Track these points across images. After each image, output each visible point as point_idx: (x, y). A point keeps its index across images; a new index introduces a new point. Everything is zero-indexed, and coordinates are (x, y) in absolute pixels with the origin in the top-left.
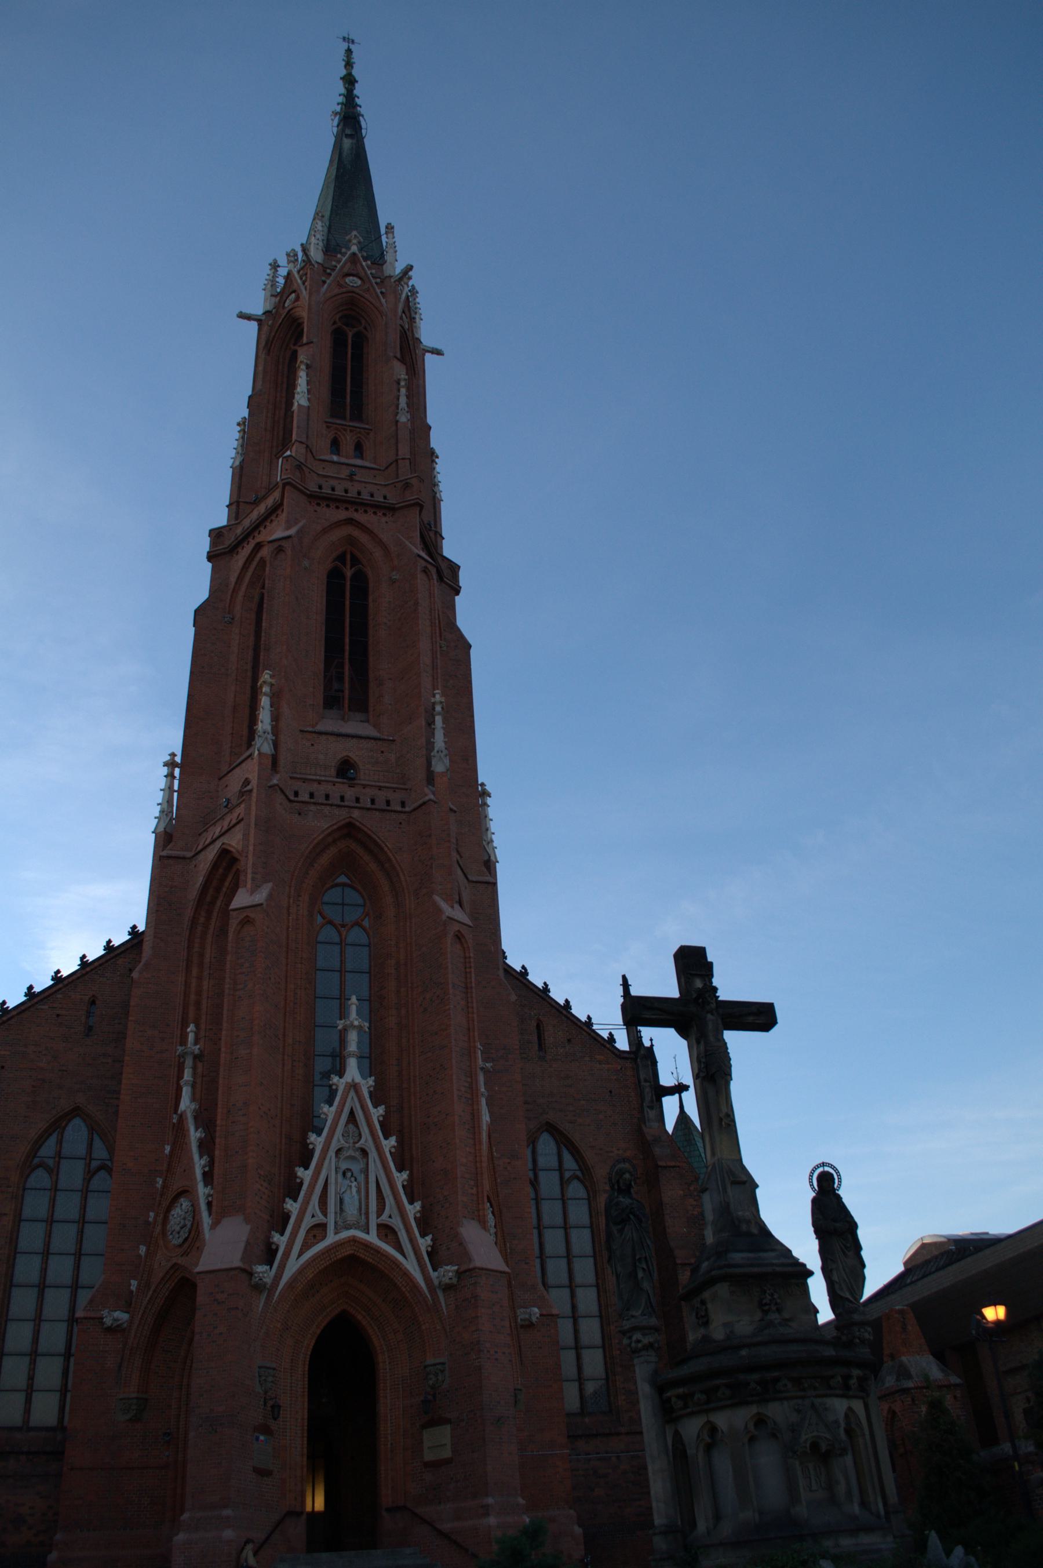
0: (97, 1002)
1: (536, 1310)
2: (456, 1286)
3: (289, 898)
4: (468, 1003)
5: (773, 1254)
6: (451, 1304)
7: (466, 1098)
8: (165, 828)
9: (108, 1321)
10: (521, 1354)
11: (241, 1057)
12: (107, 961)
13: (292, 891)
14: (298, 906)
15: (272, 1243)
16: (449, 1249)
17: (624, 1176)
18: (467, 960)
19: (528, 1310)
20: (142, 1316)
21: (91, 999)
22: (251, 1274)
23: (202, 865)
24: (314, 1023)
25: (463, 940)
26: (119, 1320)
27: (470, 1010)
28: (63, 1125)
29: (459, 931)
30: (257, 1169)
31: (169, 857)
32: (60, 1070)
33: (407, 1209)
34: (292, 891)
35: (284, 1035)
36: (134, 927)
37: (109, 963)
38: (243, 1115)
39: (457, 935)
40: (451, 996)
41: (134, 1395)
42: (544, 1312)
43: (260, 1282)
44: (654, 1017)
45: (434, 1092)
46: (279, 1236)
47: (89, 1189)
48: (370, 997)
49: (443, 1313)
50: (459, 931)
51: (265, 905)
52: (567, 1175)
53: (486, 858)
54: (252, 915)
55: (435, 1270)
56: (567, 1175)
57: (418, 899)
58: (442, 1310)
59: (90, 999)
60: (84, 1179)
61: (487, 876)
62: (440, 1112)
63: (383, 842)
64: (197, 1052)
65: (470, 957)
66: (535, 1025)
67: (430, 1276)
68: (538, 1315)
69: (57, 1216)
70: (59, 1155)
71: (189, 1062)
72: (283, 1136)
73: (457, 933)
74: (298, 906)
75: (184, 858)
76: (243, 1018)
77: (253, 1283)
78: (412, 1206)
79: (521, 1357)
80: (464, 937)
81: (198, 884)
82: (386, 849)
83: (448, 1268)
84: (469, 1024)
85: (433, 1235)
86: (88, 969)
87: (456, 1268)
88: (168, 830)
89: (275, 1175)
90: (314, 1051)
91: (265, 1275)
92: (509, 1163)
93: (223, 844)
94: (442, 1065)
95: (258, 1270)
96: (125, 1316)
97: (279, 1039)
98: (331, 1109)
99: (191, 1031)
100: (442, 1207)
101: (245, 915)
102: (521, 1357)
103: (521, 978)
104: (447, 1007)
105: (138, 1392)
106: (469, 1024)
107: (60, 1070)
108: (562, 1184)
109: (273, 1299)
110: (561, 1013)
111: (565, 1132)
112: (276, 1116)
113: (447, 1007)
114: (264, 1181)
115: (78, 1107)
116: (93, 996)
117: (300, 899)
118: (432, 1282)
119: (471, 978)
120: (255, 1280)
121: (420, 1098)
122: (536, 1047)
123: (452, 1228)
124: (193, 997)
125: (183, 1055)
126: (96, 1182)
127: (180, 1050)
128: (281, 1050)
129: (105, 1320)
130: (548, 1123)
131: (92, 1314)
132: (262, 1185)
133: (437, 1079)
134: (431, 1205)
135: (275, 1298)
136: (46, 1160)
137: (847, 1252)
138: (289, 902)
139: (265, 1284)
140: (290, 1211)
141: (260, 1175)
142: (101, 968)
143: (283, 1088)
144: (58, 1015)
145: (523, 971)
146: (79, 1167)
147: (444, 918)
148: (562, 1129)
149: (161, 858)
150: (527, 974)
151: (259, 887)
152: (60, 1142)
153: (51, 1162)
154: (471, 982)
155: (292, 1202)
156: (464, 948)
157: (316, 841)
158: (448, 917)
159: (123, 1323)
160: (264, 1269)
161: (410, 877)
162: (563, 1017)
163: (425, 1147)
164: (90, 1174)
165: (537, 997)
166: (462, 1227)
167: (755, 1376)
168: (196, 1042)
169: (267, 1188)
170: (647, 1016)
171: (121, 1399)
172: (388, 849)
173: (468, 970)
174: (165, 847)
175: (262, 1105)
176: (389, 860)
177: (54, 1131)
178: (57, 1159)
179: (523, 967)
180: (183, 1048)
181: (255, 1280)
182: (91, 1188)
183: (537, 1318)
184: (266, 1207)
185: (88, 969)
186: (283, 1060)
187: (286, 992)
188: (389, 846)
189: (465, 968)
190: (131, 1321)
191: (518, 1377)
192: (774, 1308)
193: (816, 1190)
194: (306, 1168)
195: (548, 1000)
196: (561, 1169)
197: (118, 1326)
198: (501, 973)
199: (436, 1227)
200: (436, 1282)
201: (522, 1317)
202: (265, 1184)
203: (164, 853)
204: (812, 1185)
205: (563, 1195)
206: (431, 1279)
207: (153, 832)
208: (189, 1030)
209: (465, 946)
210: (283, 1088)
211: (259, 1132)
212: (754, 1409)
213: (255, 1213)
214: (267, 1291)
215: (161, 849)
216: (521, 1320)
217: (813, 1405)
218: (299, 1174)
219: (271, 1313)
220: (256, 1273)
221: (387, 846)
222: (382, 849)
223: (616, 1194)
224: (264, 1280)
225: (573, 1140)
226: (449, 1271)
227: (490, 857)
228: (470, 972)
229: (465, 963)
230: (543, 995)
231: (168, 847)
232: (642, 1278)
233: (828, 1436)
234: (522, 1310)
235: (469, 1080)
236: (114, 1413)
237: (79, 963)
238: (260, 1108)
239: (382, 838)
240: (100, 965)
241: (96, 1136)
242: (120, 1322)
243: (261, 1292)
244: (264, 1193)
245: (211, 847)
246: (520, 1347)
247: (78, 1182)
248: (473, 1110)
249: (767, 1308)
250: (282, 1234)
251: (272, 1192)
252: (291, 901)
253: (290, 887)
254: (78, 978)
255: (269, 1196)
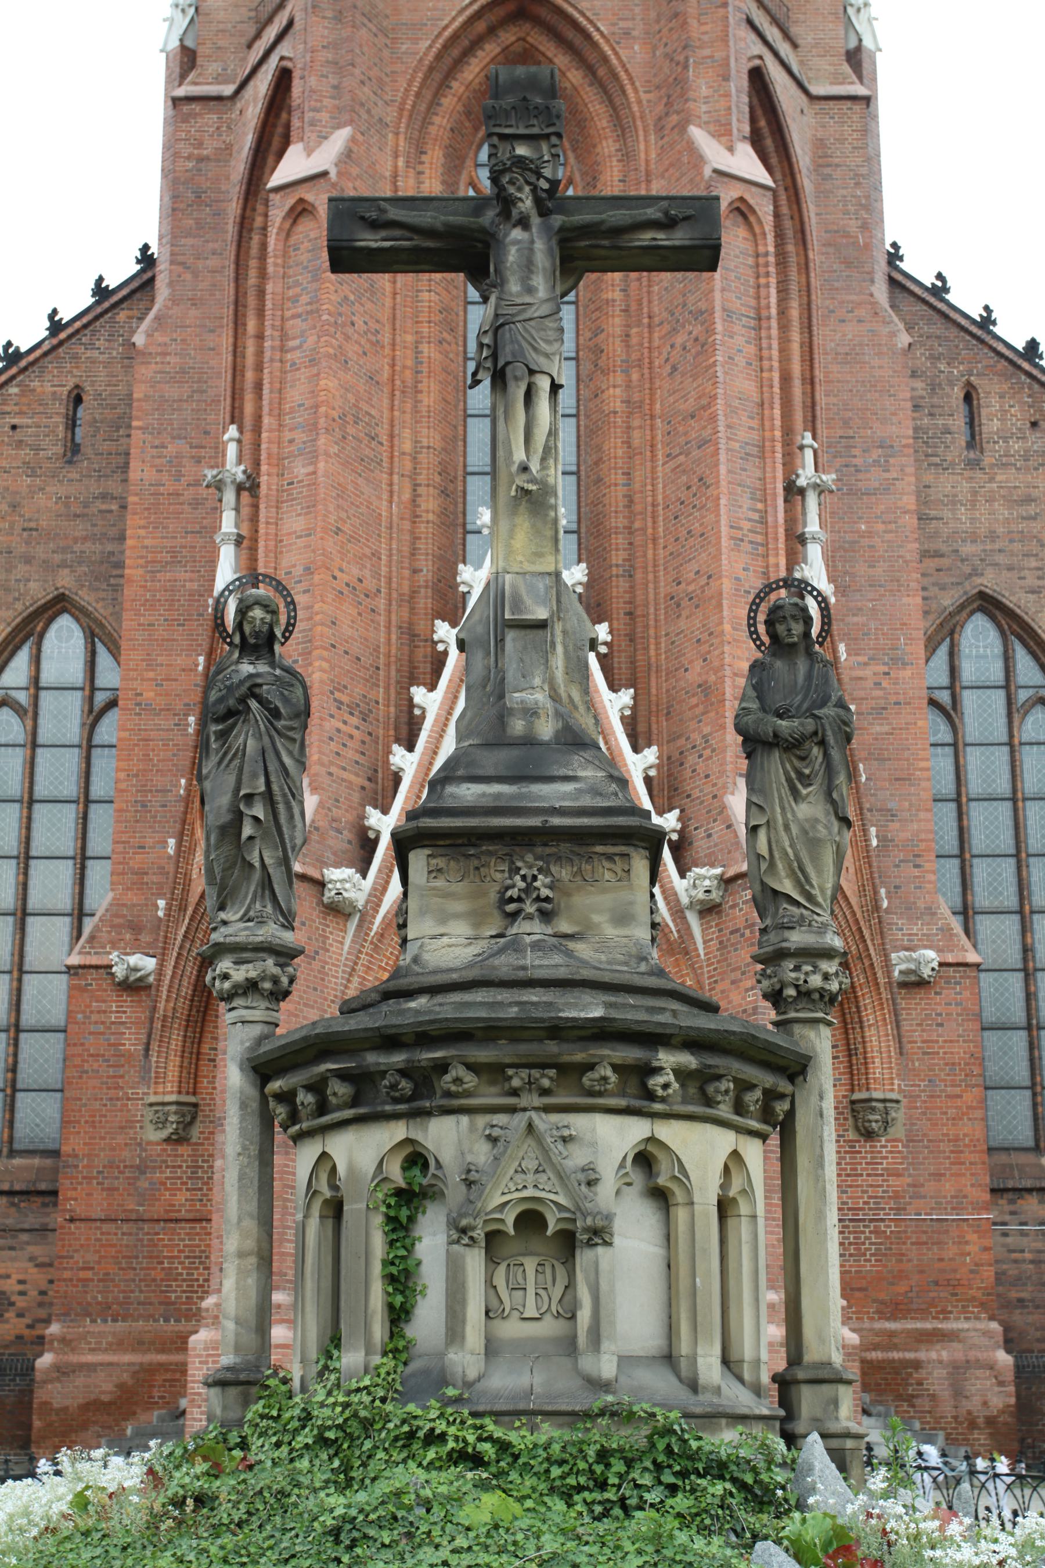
0: (84, 398)
1: (931, 954)
2: (720, 905)
3: (396, 156)
4: (761, 350)
5: (569, 787)
6: (712, 940)
7: (751, 542)
8: (181, 40)
9: (119, 971)
10: (899, 1035)
11: (299, 482)
12: (97, 318)
13: (402, 143)
14: (420, 173)
15: (370, 828)
16: (709, 836)
17: (251, 614)
18: (761, 260)
19: (914, 955)
20: (176, 962)
21: (73, 395)
22: (321, 884)
23: (250, 109)
24: (465, 410)
25: (752, 219)
26: (139, 970)
27: (766, 363)
28: (39, 629)
29: (741, 199)
30: (332, 693)
31: (190, 99)
32: (24, 530)
33: (629, 762)
34: (402, 143)
35: (392, 436)
36: (146, 248)
37: (102, 320)
38: (305, 592)
39: (738, 209)
40: (718, 337)
41: (173, 1098)
42: (950, 958)
43: (337, 898)
44: (387, 244)
45: (689, 532)
46: (380, 815)
47: (94, 743)
48: (577, 352)
49: (699, 955)
50: (741, 199)
51: (333, 174)
52: (1023, 695)
53: (853, 44)
54: (310, 197)
55: (682, 876)
56: (1023, 695)
57: (662, 138)
58: (696, 949)
59: (70, 392)
60: (83, 724)
61: (852, 83)
62: (698, 572)
63: (591, 22)
64: (240, 477)
65: (767, 254)
66: (962, 395)
67: (673, 888)
68: (935, 964)
69: (40, 792)
70: (35, 684)
71: (229, 496)
72: (394, 629)
73: (738, 204)
74: (420, 173)
75: (219, 98)
76: (299, 406)
77: (325, 900)
78: (640, 756)
79: (900, 1042)
80: (754, 212)
81: (248, 145)
82: (596, 36)
83: (702, 871)
84: (762, 393)
85: (682, 811)
86: (63, 335)
87: (718, 871)
88: (189, 43)
89: (377, 703)
90: (465, 466)
91: (347, 886)
92: (886, 674)
93: (282, 58)
94: (701, 480)
95: (334, 877)
96: (149, 964)
97: (381, 444)
98: (477, 573)
99: (231, 440)
100: (700, 756)
101: (297, 197)
102: (900, 1042)
103: (932, 300)
104: (712, 360)
105: (180, 1092)
106: (762, 393)
107: (24, 530)
108: (1010, 715)
109: (371, 929)
110: (1019, 368)
111: (1018, 611)
112: (379, 591)
113: (712, 360)
114: (352, 714)
115: (63, 594)
116: (77, 387)
117: (424, 158)
118: (678, 901)
119: (768, 297)
120: (329, 894)
121: (665, 547)
122: (962, 440)
123: (715, 797)
124: (250, 375)
125: (218, 485)
126: (108, 730)
127: (209, 477)
128: (385, 465)
129: (114, 969)
130: (982, 595)
131: (94, 960)
132: (345, 723)
133: (694, 507)
134: (681, 753)
135: (375, 928)
136: (13, 694)
137: (800, 786)
138: (396, 167)
139: (352, 904)
140: (402, 769)
141: (342, 703)
142: (86, 332)
143: (391, 538)
144: (14, 427)
145: (939, 284)
146: (74, 702)
147: (707, 172)
148: (1011, 605)
149: (176, 102)
150: (947, 290)
151: (326, 138)
152: (36, 660)
153: (22, 697)
154: (768, 307)
155: (405, 752)
156: (754, 235)
157: (447, 33)
158: (716, 171)
159: (149, 975)
160: (345, 876)
161: (649, 92)
162: (1023, 377)
163: (673, 643)
164: (94, 716)
165: (968, 338)
166: (733, 794)
167: (398, 1058)
168: (239, 461)
169: (357, 728)
170: (373, 245)
171: (151, 1105)
172: (602, 34)
173: (762, 281)
174: (183, 77)
175: (341, 570)
176: (605, 59)
177: (23, 642)
178: (32, 691)
179: (940, 276)
180: (215, 472)
181: (329, 894)
182: (97, 740)
183: (933, 969)
184: (357, 763)
185: (63, 335)
186: (391, 484)
187: (394, 350)
188: (602, 28)
189: (758, 277)
190: (160, 971)
191: (892, 1079)
192: (530, 908)
193: (763, 644)
194: (432, 687)
195: (992, 342)
196: (1008, 685)
197: (140, 979)
198: (881, 291)
199: (689, 796)
200: (685, 900)
201: (903, 967)
202: (354, 721)
203: (181, 92)
204: (753, 634)
205: (1011, 735)
206: (676, 894)
207: (162, 51)
208: (226, 437)
209: (757, 230)
210: (391, 538)
211: (334, 623)
212: (399, 1131)
213: (330, 774)
214: (358, 915)
215: (176, 83)
216: (901, 972)
217: (530, 1127)
218: (417, 700)
219: (367, 954)
220: (330, 882)
221: (598, 29)
222: (588, 37)
223: (236, 655)
224: (346, 895)
225: (1036, 627)
226: (705, 878)
227: (860, 40)
228: (767, 286)
229: (757, 265)
230: (979, 332)
231: (189, 79)
232: (251, 838)
233: (561, 1200)
234: (903, 954)
235: (760, 506)
236: (141, 1128)
237: (48, 324)
238: (335, 578)
239: (588, 14)
240: (85, 326)
241: (100, 649)
242: (142, 973)
243: (348, 916)
244: (351, 737)
245: (264, 68)
246: (897, 1022)
247: (73, 730)
248: (767, 567)
249: (511, 907)
250: (385, 811)
251: (370, 734)
252: (401, 163)
253: (397, 134)
254: (45, 354)
255: (363, 742)
